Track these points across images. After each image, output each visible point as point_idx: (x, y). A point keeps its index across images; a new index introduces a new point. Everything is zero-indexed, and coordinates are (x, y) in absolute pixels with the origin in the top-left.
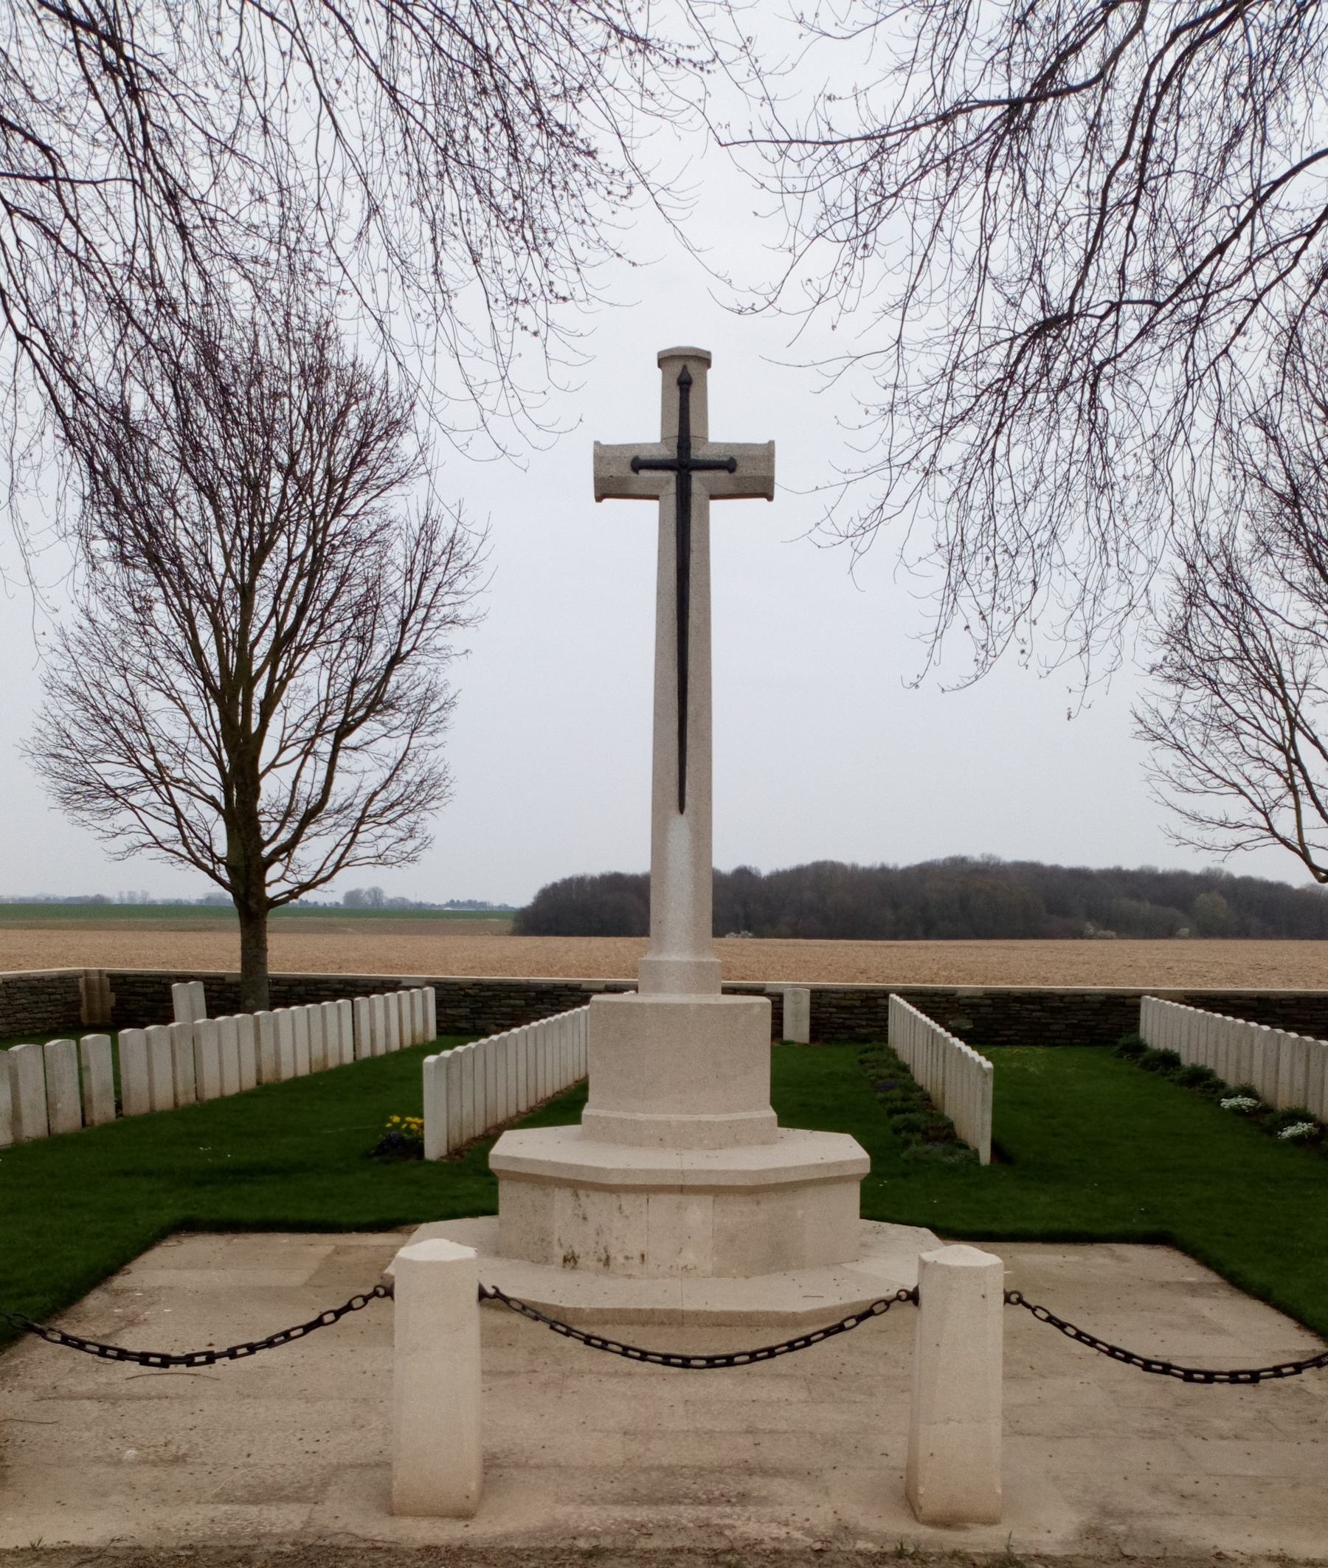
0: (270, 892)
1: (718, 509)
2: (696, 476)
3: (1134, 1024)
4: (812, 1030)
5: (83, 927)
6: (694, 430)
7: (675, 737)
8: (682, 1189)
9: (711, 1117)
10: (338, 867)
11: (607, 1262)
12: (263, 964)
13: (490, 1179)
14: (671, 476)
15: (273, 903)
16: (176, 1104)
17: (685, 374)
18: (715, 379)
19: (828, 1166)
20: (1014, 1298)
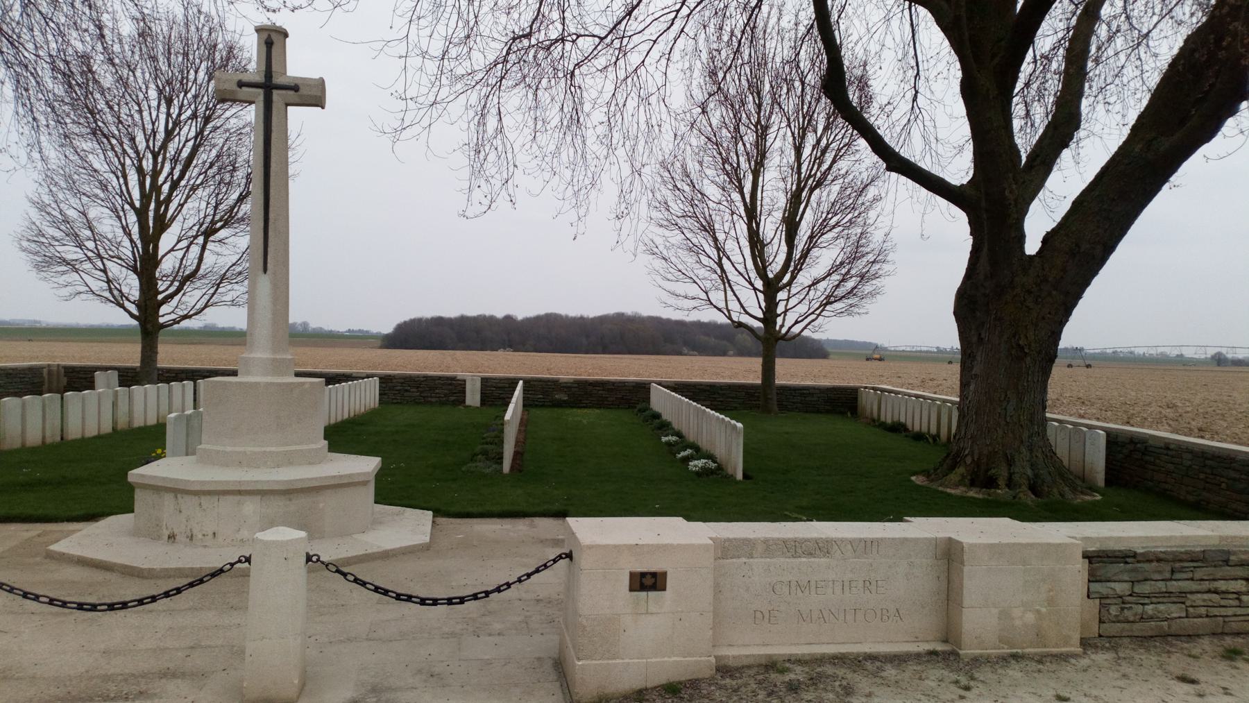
0: (161, 320)
2: (275, 92)
3: (647, 399)
4: (482, 400)
5: (126, 342)
6: (275, 68)
8: (240, 492)
9: (273, 449)
10: (206, 306)
11: (191, 538)
12: (155, 361)
13: (131, 488)
14: (261, 91)
15: (163, 326)
16: (43, 442)
19: (341, 476)
20: (314, 559)
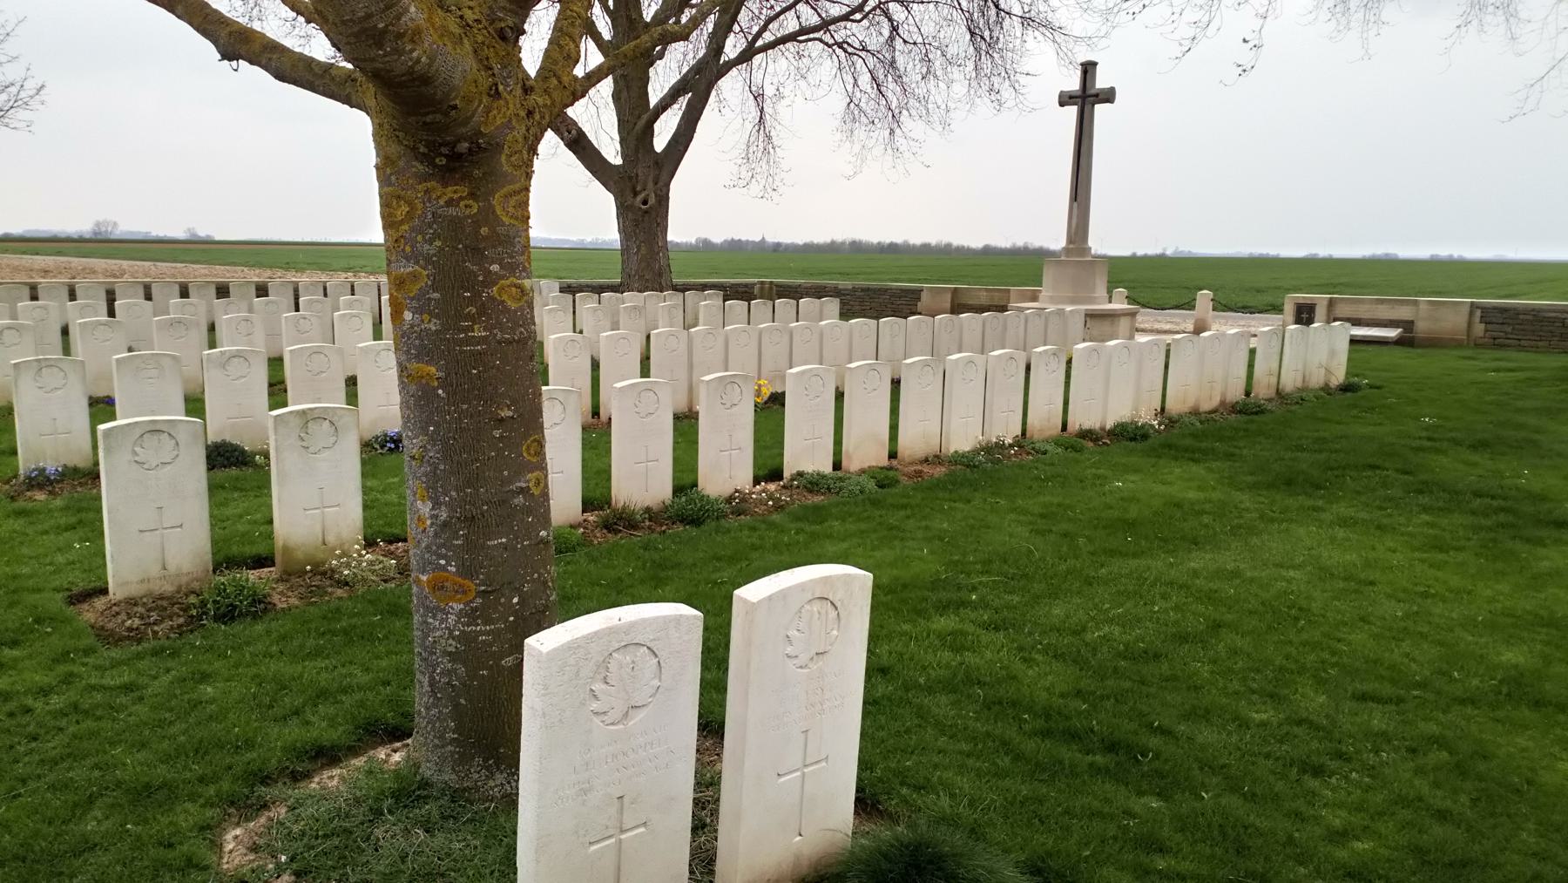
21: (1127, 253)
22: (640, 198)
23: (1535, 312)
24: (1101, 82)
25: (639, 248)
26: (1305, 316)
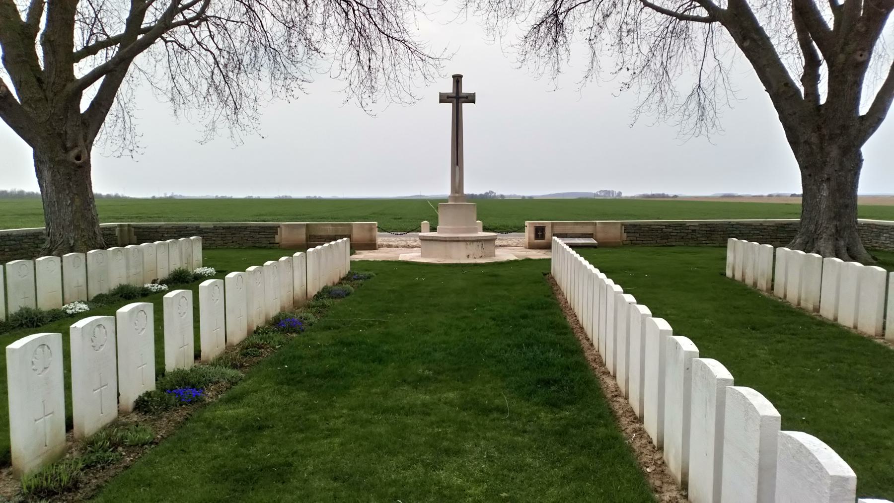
1: (464, 105)
7: (727, 434)
17: (457, 80)
18: (464, 81)
21: (149, 196)
22: (73, 154)
23: (648, 226)
24: (466, 89)
25: (73, 200)
26: (540, 233)
